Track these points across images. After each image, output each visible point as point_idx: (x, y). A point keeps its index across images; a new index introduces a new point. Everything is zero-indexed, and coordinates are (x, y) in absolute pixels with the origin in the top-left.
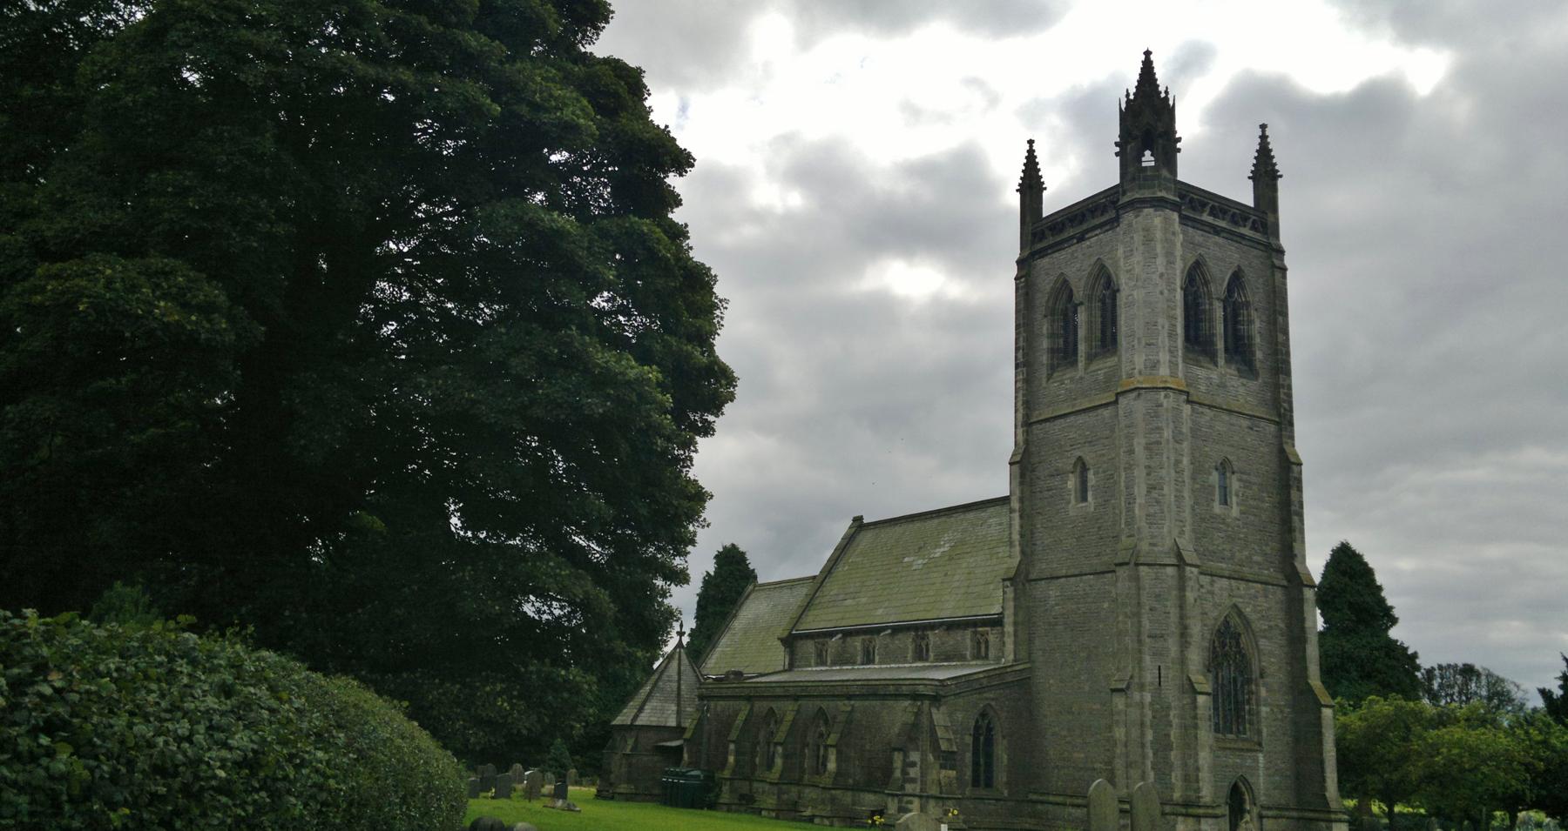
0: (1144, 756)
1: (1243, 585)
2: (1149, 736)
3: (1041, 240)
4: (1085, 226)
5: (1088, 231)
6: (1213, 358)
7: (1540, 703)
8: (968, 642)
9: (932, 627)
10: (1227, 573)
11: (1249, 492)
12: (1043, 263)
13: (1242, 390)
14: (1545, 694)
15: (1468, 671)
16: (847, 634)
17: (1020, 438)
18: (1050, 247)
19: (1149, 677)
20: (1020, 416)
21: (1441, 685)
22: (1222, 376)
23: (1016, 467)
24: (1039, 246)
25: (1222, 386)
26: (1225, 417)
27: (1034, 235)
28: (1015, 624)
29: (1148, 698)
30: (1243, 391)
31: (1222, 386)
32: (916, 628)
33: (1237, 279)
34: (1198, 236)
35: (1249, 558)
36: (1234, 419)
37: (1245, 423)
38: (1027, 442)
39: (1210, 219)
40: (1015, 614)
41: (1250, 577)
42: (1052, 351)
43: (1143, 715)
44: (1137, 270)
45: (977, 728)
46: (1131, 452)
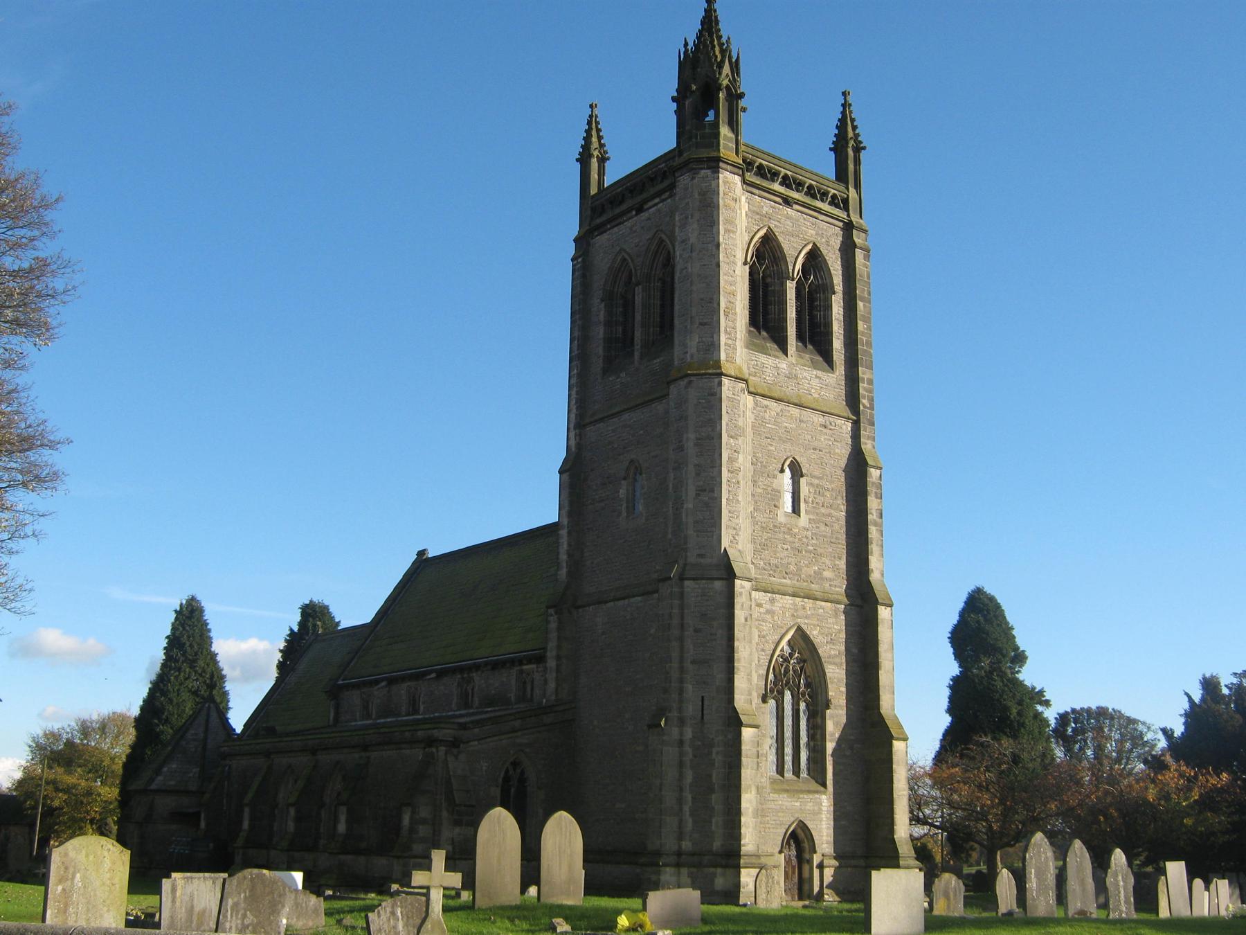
0: (680, 801)
1: (809, 603)
2: (689, 777)
3: (601, 215)
4: (644, 196)
5: (646, 201)
6: (783, 346)
7: (1162, 743)
8: (513, 682)
9: (477, 667)
10: (790, 590)
11: (820, 499)
12: (602, 240)
13: (815, 382)
14: (1167, 733)
15: (1102, 713)
16: (391, 681)
17: (573, 443)
18: (609, 221)
19: (691, 709)
20: (573, 416)
21: (1074, 730)
22: (791, 365)
23: (566, 476)
24: (598, 221)
25: (791, 377)
26: (795, 411)
27: (593, 210)
28: (558, 658)
29: (689, 733)
30: (825, 384)
31: (791, 377)
32: (461, 670)
33: (814, 259)
34: (767, 206)
35: (818, 574)
36: (806, 414)
37: (818, 419)
38: (579, 446)
39: (782, 189)
40: (559, 647)
41: (818, 595)
42: (609, 341)
43: (681, 754)
44: (693, 240)
45: (507, 779)
46: (681, 448)
